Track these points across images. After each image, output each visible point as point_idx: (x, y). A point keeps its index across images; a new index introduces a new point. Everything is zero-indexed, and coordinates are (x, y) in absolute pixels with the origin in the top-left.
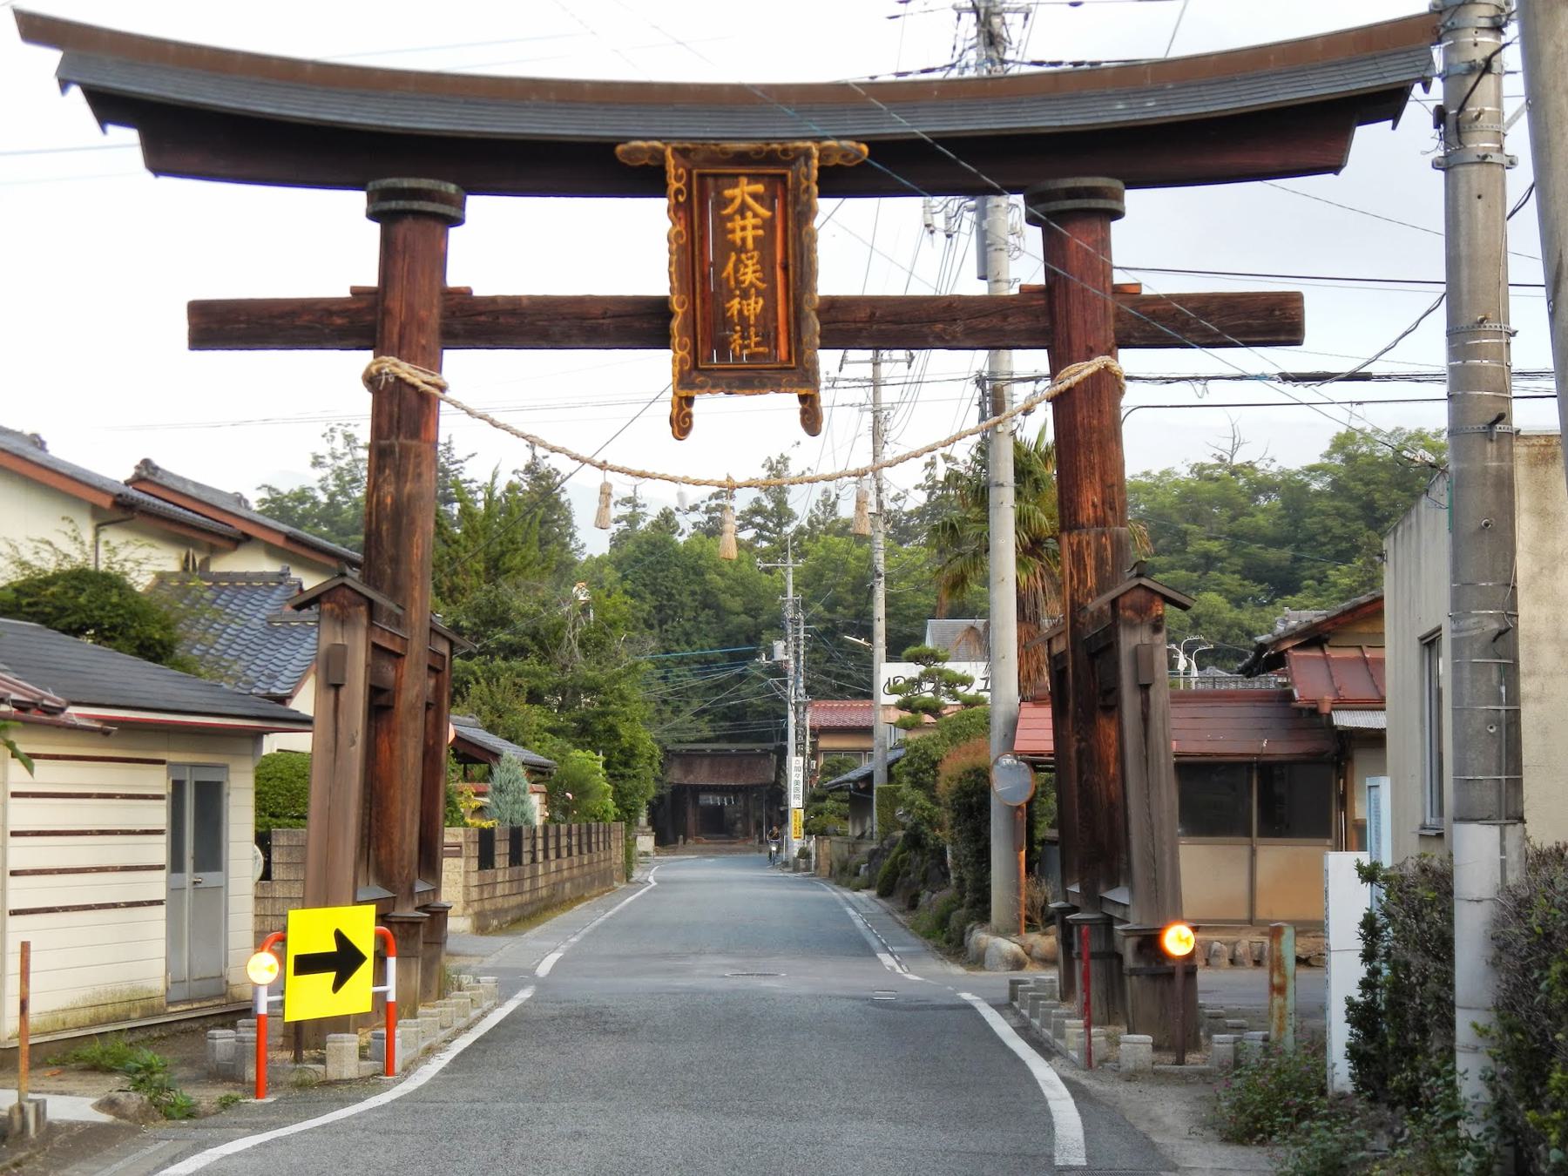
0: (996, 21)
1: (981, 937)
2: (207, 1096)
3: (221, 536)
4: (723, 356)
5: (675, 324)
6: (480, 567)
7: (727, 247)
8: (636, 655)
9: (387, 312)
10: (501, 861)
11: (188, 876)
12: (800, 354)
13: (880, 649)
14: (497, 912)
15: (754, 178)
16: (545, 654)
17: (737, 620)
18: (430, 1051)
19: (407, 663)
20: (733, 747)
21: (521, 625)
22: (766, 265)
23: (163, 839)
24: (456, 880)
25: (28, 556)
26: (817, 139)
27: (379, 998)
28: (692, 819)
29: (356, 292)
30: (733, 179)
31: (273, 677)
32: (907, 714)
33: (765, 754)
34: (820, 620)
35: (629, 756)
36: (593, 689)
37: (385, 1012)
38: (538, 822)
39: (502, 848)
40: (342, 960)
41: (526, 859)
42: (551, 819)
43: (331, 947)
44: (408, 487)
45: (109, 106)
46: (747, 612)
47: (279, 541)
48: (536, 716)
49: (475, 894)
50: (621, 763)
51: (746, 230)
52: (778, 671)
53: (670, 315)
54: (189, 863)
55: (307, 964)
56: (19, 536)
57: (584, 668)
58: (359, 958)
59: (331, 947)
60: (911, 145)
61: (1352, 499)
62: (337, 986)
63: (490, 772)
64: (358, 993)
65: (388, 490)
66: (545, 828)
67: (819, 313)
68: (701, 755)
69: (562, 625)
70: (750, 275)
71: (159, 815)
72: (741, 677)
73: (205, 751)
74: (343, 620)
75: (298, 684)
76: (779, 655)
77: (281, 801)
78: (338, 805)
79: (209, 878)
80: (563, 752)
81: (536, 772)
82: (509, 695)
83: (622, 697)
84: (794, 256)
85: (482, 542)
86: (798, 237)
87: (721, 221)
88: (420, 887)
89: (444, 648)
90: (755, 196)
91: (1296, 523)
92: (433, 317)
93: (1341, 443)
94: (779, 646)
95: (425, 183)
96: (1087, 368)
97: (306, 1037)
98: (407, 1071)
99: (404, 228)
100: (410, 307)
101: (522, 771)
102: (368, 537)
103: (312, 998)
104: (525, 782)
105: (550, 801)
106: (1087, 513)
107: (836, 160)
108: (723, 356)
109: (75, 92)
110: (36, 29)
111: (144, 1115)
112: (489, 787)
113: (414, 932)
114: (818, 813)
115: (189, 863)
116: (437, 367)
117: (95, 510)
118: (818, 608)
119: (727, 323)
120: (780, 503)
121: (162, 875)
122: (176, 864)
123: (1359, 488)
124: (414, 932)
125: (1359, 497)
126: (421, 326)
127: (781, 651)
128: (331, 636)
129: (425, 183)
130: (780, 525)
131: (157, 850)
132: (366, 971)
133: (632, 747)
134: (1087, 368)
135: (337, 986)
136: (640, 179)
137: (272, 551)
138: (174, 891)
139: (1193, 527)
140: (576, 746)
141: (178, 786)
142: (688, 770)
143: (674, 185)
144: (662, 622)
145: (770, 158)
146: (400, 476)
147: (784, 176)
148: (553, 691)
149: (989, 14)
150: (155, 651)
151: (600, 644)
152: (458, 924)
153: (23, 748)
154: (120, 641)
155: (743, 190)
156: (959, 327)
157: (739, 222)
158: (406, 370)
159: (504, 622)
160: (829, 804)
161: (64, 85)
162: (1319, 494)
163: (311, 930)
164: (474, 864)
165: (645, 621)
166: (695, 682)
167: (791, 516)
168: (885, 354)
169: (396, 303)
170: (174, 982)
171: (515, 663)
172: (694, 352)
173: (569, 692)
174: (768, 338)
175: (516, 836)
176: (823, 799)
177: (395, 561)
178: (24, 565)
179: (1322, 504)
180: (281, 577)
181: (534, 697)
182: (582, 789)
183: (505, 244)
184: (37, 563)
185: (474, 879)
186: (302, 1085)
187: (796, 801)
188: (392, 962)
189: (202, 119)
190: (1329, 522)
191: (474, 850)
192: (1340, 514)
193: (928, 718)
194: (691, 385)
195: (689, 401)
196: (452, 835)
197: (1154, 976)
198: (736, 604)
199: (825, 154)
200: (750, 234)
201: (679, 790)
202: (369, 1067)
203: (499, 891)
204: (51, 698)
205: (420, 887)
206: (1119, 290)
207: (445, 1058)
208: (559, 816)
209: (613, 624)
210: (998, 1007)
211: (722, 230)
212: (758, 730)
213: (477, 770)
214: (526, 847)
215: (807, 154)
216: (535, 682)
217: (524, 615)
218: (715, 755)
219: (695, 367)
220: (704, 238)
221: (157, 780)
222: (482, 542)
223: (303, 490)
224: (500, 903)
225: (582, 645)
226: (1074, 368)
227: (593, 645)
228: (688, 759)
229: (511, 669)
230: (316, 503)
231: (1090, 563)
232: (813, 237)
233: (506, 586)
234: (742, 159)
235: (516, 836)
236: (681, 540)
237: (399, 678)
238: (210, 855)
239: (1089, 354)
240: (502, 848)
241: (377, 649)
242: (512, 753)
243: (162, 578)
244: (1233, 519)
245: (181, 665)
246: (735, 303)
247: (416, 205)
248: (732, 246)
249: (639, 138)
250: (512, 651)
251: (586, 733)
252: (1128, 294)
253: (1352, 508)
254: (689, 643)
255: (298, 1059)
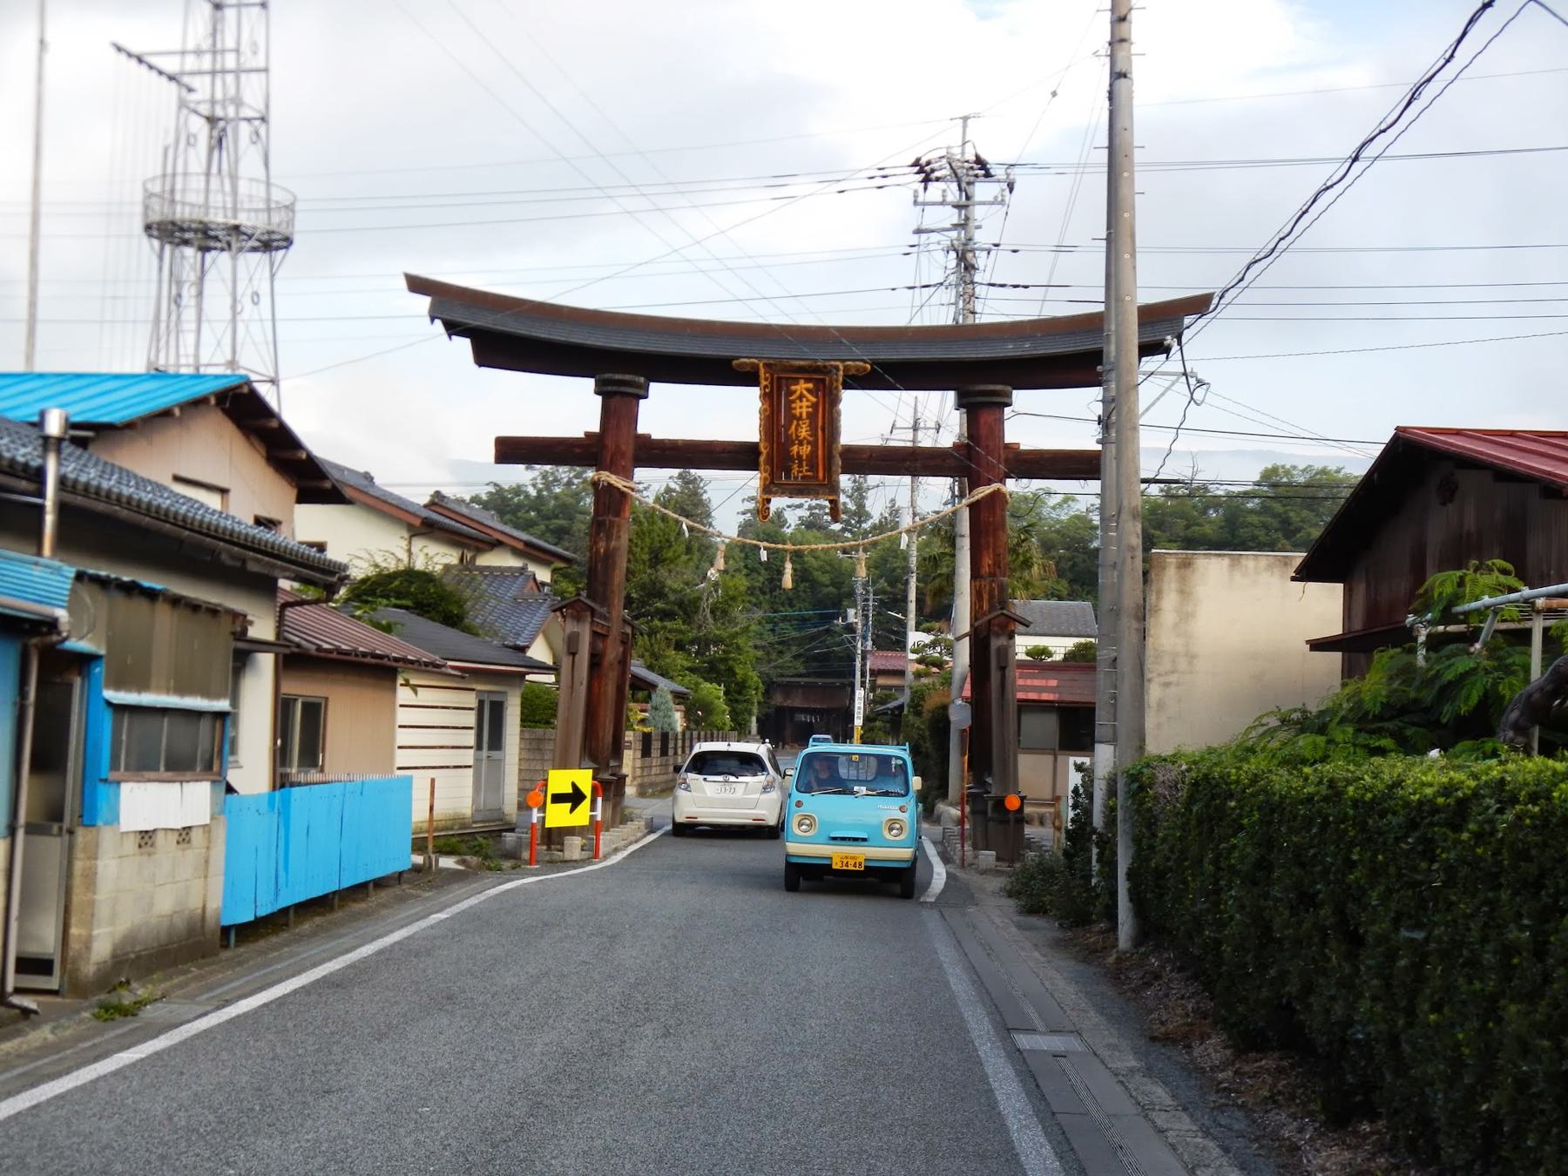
0: (969, 255)
1: (941, 807)
2: (507, 864)
3: (483, 541)
4: (788, 477)
5: (762, 459)
6: (646, 557)
7: (791, 417)
8: (748, 619)
9: (604, 446)
10: (655, 753)
11: (485, 753)
12: (830, 477)
13: (912, 622)
14: (652, 785)
15: (807, 380)
16: (688, 619)
17: (826, 590)
18: (616, 850)
19: (609, 641)
20: (820, 681)
21: (672, 597)
22: (813, 428)
23: (473, 732)
24: (630, 761)
25: (379, 560)
26: (843, 361)
27: (592, 817)
28: (788, 732)
29: (588, 434)
30: (796, 381)
31: (518, 634)
32: (922, 667)
33: (843, 686)
34: (884, 592)
35: (742, 687)
36: (718, 641)
37: (595, 827)
38: (679, 730)
39: (656, 745)
40: (575, 798)
41: (671, 752)
42: (687, 728)
43: (570, 791)
44: (613, 543)
45: (453, 328)
46: (833, 584)
47: (520, 546)
48: (679, 659)
49: (638, 772)
50: (736, 692)
51: (802, 408)
52: (850, 628)
53: (759, 453)
54: (485, 745)
55: (558, 798)
56: (373, 549)
57: (712, 627)
58: (583, 797)
59: (570, 791)
60: (898, 363)
61: (1275, 516)
62: (572, 810)
63: (649, 697)
64: (582, 816)
65: (602, 546)
66: (684, 734)
67: (841, 455)
68: (798, 685)
69: (700, 599)
70: (804, 432)
71: (470, 719)
72: (828, 631)
73: (496, 684)
74: (578, 619)
75: (532, 639)
76: (851, 619)
77: (538, 713)
78: (572, 713)
79: (495, 754)
80: (697, 684)
81: (679, 697)
82: (663, 644)
83: (738, 648)
84: (828, 422)
85: (648, 540)
86: (831, 413)
87: (789, 403)
88: (612, 763)
89: (629, 630)
90: (808, 390)
91: (1233, 532)
92: (628, 448)
93: (1269, 476)
94: (851, 612)
95: (627, 377)
96: (983, 491)
97: (554, 837)
98: (606, 857)
99: (614, 401)
100: (618, 446)
101: (670, 697)
102: (590, 569)
103: (558, 816)
104: (671, 704)
105: (688, 715)
106: (985, 570)
107: (853, 372)
108: (788, 477)
109: (438, 323)
110: (417, 285)
111: (480, 867)
112: (649, 706)
113: (610, 787)
114: (871, 729)
115: (485, 745)
116: (630, 477)
117: (410, 527)
118: (883, 583)
119: (792, 459)
120: (861, 506)
121: (472, 752)
122: (479, 747)
123: (1278, 507)
124: (610, 787)
125: (1279, 515)
126: (623, 455)
127: (853, 615)
128: (571, 627)
129: (627, 377)
130: (860, 522)
131: (470, 738)
132: (586, 803)
133: (744, 681)
134: (983, 491)
135: (572, 810)
136: (745, 378)
137: (516, 552)
138: (477, 760)
139: (1157, 533)
140: (706, 680)
141: (481, 703)
142: (787, 696)
143: (764, 383)
144: (772, 591)
145: (817, 370)
146: (609, 538)
147: (823, 381)
148: (692, 643)
149: (964, 253)
150: (453, 620)
151: (725, 613)
152: (630, 790)
153: (412, 682)
154: (433, 614)
155: (802, 387)
156: (918, 464)
157: (798, 404)
158: (614, 480)
159: (660, 595)
160: (878, 724)
161: (432, 319)
162: (1252, 511)
163: (560, 781)
164: (639, 754)
165: (761, 589)
166: (794, 634)
167: (869, 516)
168: (910, 444)
169: (610, 442)
170: (476, 811)
171: (668, 624)
172: (772, 474)
173: (704, 643)
174: (813, 467)
175: (665, 737)
176: (874, 720)
177: (605, 584)
178: (377, 566)
179: (1254, 519)
180: (524, 569)
181: (679, 646)
182: (708, 708)
183: (670, 411)
184: (384, 565)
185: (638, 763)
186: (551, 862)
187: (858, 722)
188: (600, 800)
189: (506, 336)
190: (1257, 532)
191: (639, 746)
192: (1265, 526)
193: (935, 670)
194: (770, 492)
195: (769, 501)
196: (629, 736)
197: (1001, 822)
198: (825, 579)
199: (846, 369)
200: (804, 410)
201: (780, 710)
202: (585, 854)
203: (654, 771)
204: (438, 660)
205: (612, 763)
206: (1008, 446)
207: (626, 853)
208: (693, 726)
209: (733, 598)
210: (935, 843)
211: (789, 408)
212: (835, 669)
213: (640, 695)
214: (671, 745)
215: (837, 368)
216: (680, 637)
217: (675, 591)
218: (807, 686)
219: (772, 482)
220: (779, 411)
221: (470, 700)
222: (648, 540)
223: (519, 486)
224: (653, 779)
225: (712, 612)
226: (981, 489)
227: (720, 612)
228: (788, 689)
229: (664, 628)
230: (527, 496)
231: (986, 596)
232: (839, 414)
233: (662, 572)
234: (801, 369)
235: (665, 737)
236: (789, 531)
237: (605, 648)
238: (496, 742)
239: (989, 483)
240: (656, 745)
241: (595, 634)
242: (664, 685)
243: (447, 567)
244: (1187, 527)
245: (468, 630)
246: (795, 448)
247: (623, 389)
248: (794, 417)
249: (746, 357)
250: (666, 615)
251: (715, 671)
252: (1012, 449)
253: (1275, 523)
254: (791, 605)
255: (549, 849)
